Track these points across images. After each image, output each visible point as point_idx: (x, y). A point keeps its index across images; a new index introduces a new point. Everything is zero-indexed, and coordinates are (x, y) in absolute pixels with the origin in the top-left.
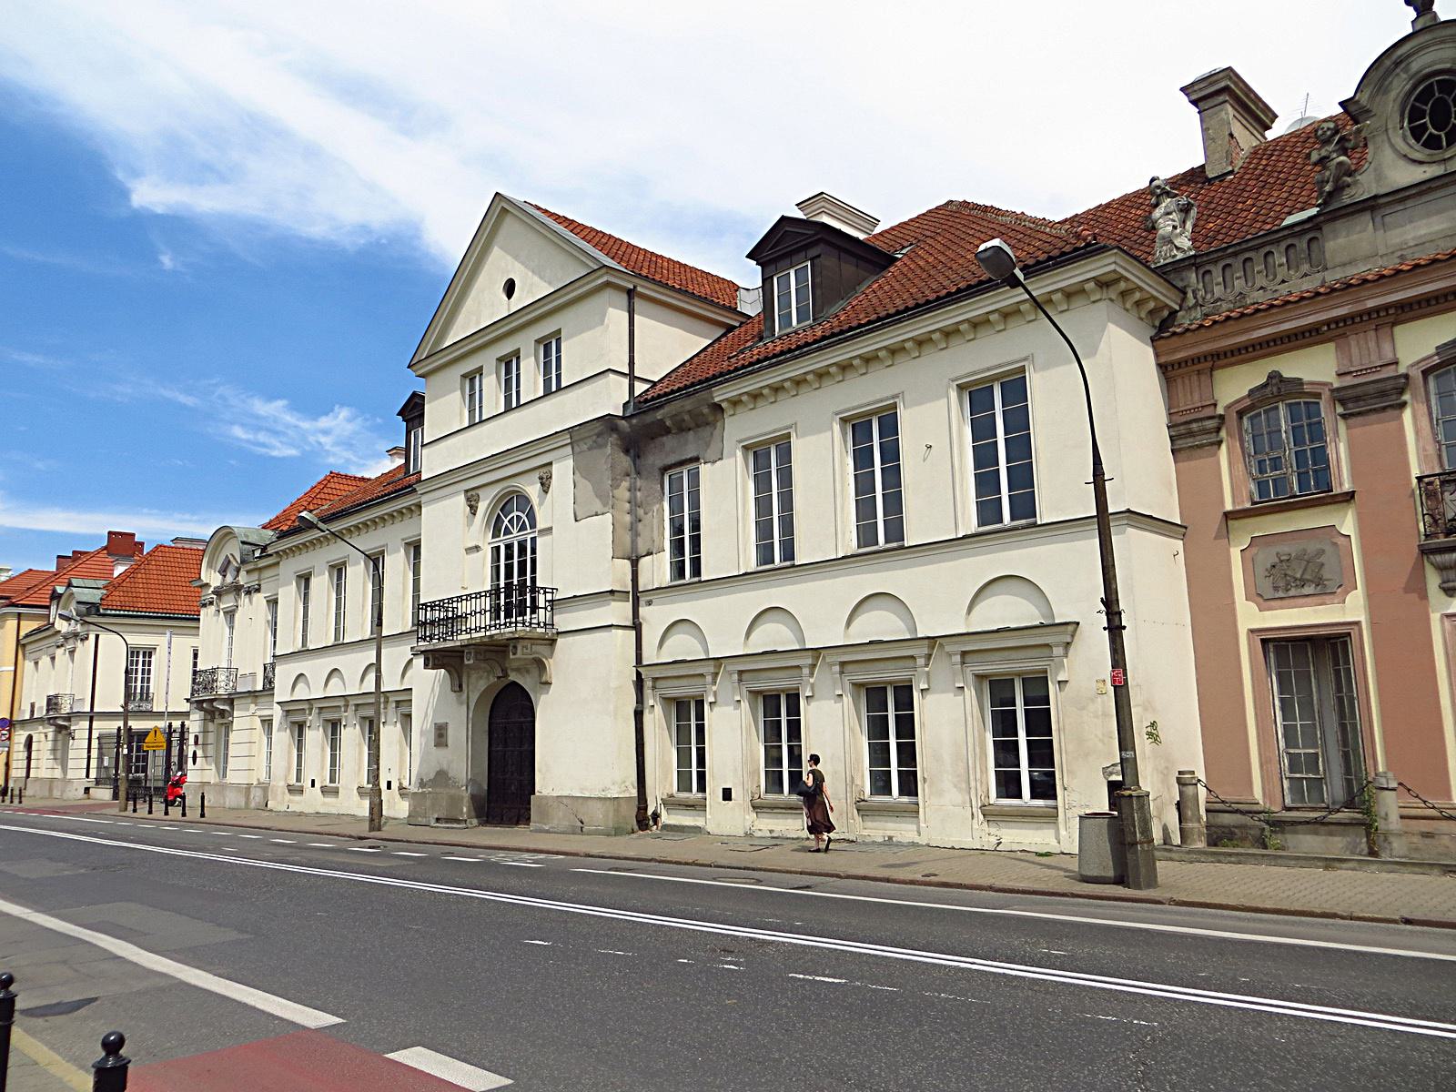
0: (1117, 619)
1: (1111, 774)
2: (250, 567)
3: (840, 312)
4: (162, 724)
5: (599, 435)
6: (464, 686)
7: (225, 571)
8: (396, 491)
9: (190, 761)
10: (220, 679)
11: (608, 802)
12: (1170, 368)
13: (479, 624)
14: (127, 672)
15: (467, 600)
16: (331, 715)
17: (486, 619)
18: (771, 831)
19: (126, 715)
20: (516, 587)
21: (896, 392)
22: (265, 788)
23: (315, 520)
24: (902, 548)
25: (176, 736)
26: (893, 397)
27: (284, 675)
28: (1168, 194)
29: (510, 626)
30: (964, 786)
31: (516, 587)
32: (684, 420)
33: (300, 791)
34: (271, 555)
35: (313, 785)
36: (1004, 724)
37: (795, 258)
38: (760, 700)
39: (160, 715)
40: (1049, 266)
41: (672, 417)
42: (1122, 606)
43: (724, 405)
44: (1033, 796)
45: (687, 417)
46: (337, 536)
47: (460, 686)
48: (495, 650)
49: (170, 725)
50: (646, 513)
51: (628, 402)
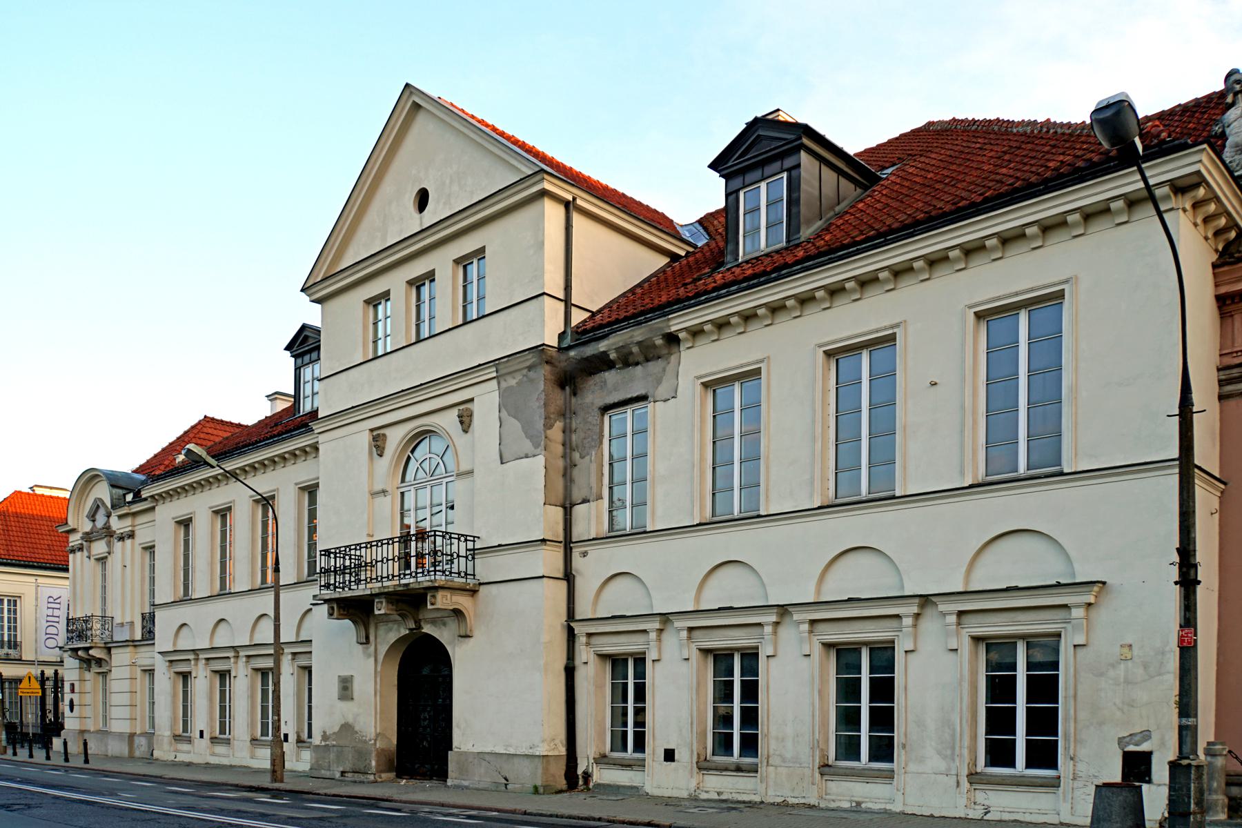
0: (1192, 572)
1: (1128, 744)
2: (124, 510)
4: (35, 671)
5: (530, 368)
6: (372, 638)
7: (94, 516)
11: (537, 760)
17: (395, 568)
18: (719, 794)
21: (898, 321)
22: (150, 736)
23: (204, 454)
24: (1062, 474)
25: (49, 685)
26: (892, 327)
27: (165, 622)
30: (949, 752)
32: (631, 353)
33: (189, 740)
34: (145, 499)
36: (849, 690)
37: (768, 170)
38: (710, 660)
39: (31, 663)
40: (1110, 167)
41: (617, 350)
42: (1198, 559)
43: (682, 335)
44: (1029, 765)
45: (635, 349)
46: (233, 475)
47: (367, 638)
48: (410, 602)
49: (43, 673)
50: (582, 457)
51: (564, 332)
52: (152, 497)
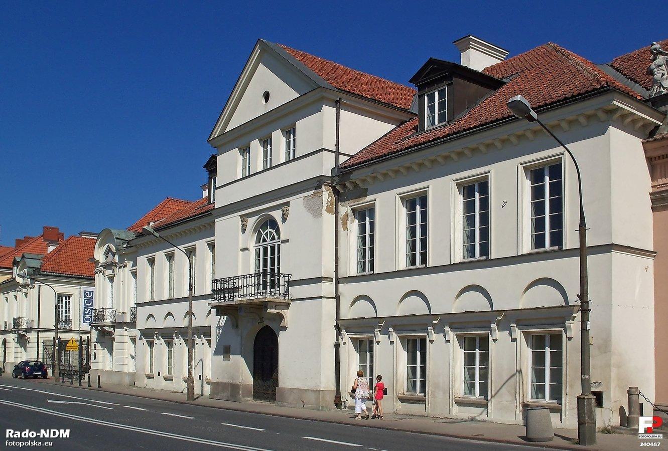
3: (465, 120)
4: (76, 336)
8: (202, 213)
9: (93, 358)
10: (106, 314)
12: (653, 159)
13: (248, 293)
14: (56, 307)
15: (249, 277)
16: (168, 335)
17: (252, 290)
19: (57, 330)
20: (269, 273)
23: (152, 231)
25: (84, 344)
27: (142, 312)
28: (661, 53)
29: (262, 295)
31: (269, 273)
35: (159, 375)
39: (75, 332)
40: (578, 99)
48: (260, 307)
52: (136, 245)
